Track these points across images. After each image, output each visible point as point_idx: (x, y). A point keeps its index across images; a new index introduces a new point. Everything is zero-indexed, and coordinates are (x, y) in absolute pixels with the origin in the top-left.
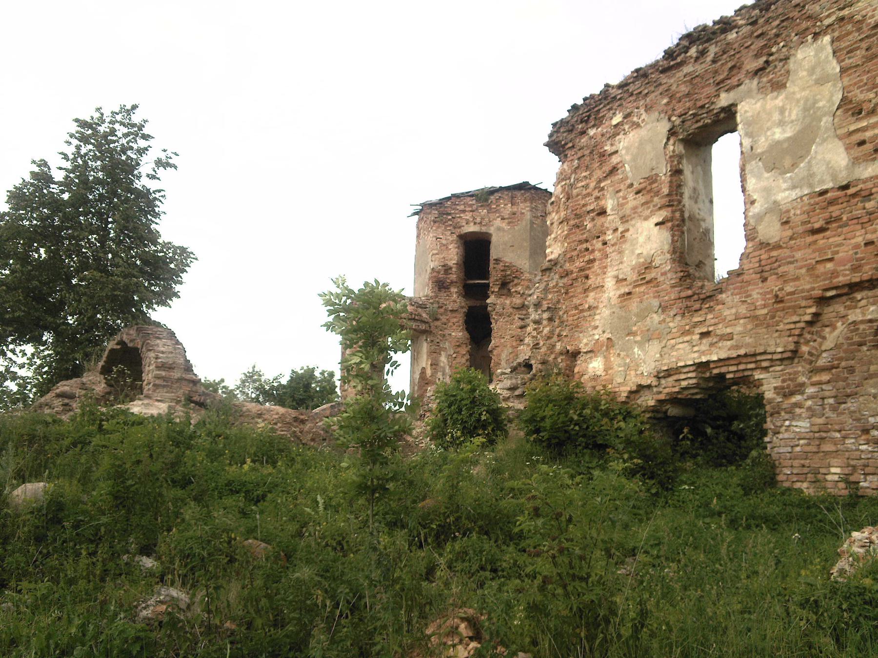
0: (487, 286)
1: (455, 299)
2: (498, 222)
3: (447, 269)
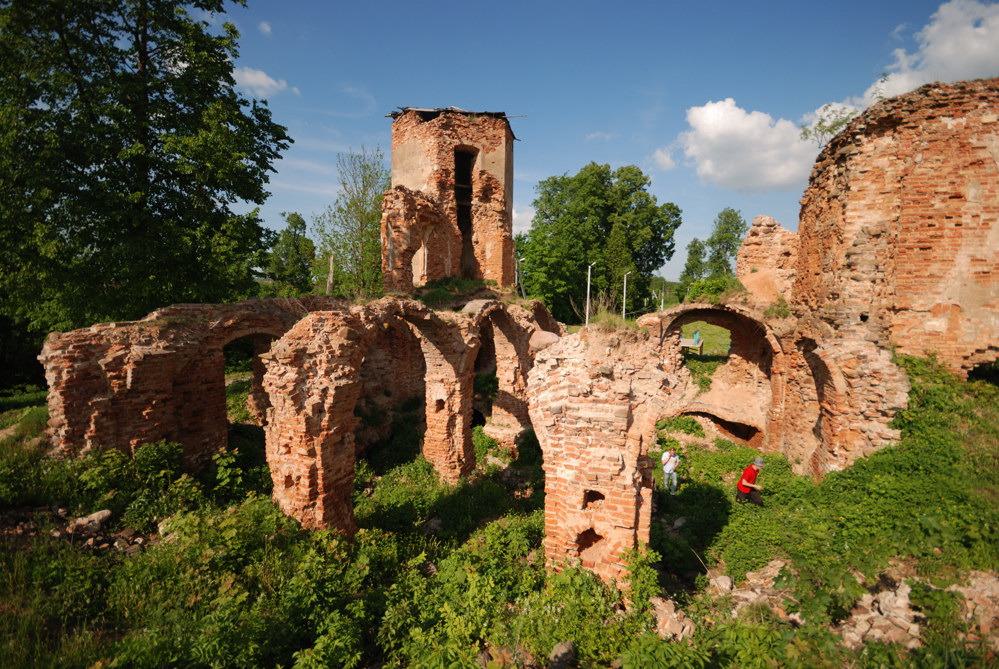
0: (471, 191)
1: (449, 205)
2: (484, 141)
3: (447, 172)
